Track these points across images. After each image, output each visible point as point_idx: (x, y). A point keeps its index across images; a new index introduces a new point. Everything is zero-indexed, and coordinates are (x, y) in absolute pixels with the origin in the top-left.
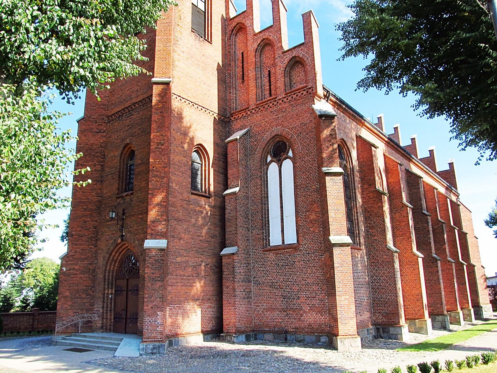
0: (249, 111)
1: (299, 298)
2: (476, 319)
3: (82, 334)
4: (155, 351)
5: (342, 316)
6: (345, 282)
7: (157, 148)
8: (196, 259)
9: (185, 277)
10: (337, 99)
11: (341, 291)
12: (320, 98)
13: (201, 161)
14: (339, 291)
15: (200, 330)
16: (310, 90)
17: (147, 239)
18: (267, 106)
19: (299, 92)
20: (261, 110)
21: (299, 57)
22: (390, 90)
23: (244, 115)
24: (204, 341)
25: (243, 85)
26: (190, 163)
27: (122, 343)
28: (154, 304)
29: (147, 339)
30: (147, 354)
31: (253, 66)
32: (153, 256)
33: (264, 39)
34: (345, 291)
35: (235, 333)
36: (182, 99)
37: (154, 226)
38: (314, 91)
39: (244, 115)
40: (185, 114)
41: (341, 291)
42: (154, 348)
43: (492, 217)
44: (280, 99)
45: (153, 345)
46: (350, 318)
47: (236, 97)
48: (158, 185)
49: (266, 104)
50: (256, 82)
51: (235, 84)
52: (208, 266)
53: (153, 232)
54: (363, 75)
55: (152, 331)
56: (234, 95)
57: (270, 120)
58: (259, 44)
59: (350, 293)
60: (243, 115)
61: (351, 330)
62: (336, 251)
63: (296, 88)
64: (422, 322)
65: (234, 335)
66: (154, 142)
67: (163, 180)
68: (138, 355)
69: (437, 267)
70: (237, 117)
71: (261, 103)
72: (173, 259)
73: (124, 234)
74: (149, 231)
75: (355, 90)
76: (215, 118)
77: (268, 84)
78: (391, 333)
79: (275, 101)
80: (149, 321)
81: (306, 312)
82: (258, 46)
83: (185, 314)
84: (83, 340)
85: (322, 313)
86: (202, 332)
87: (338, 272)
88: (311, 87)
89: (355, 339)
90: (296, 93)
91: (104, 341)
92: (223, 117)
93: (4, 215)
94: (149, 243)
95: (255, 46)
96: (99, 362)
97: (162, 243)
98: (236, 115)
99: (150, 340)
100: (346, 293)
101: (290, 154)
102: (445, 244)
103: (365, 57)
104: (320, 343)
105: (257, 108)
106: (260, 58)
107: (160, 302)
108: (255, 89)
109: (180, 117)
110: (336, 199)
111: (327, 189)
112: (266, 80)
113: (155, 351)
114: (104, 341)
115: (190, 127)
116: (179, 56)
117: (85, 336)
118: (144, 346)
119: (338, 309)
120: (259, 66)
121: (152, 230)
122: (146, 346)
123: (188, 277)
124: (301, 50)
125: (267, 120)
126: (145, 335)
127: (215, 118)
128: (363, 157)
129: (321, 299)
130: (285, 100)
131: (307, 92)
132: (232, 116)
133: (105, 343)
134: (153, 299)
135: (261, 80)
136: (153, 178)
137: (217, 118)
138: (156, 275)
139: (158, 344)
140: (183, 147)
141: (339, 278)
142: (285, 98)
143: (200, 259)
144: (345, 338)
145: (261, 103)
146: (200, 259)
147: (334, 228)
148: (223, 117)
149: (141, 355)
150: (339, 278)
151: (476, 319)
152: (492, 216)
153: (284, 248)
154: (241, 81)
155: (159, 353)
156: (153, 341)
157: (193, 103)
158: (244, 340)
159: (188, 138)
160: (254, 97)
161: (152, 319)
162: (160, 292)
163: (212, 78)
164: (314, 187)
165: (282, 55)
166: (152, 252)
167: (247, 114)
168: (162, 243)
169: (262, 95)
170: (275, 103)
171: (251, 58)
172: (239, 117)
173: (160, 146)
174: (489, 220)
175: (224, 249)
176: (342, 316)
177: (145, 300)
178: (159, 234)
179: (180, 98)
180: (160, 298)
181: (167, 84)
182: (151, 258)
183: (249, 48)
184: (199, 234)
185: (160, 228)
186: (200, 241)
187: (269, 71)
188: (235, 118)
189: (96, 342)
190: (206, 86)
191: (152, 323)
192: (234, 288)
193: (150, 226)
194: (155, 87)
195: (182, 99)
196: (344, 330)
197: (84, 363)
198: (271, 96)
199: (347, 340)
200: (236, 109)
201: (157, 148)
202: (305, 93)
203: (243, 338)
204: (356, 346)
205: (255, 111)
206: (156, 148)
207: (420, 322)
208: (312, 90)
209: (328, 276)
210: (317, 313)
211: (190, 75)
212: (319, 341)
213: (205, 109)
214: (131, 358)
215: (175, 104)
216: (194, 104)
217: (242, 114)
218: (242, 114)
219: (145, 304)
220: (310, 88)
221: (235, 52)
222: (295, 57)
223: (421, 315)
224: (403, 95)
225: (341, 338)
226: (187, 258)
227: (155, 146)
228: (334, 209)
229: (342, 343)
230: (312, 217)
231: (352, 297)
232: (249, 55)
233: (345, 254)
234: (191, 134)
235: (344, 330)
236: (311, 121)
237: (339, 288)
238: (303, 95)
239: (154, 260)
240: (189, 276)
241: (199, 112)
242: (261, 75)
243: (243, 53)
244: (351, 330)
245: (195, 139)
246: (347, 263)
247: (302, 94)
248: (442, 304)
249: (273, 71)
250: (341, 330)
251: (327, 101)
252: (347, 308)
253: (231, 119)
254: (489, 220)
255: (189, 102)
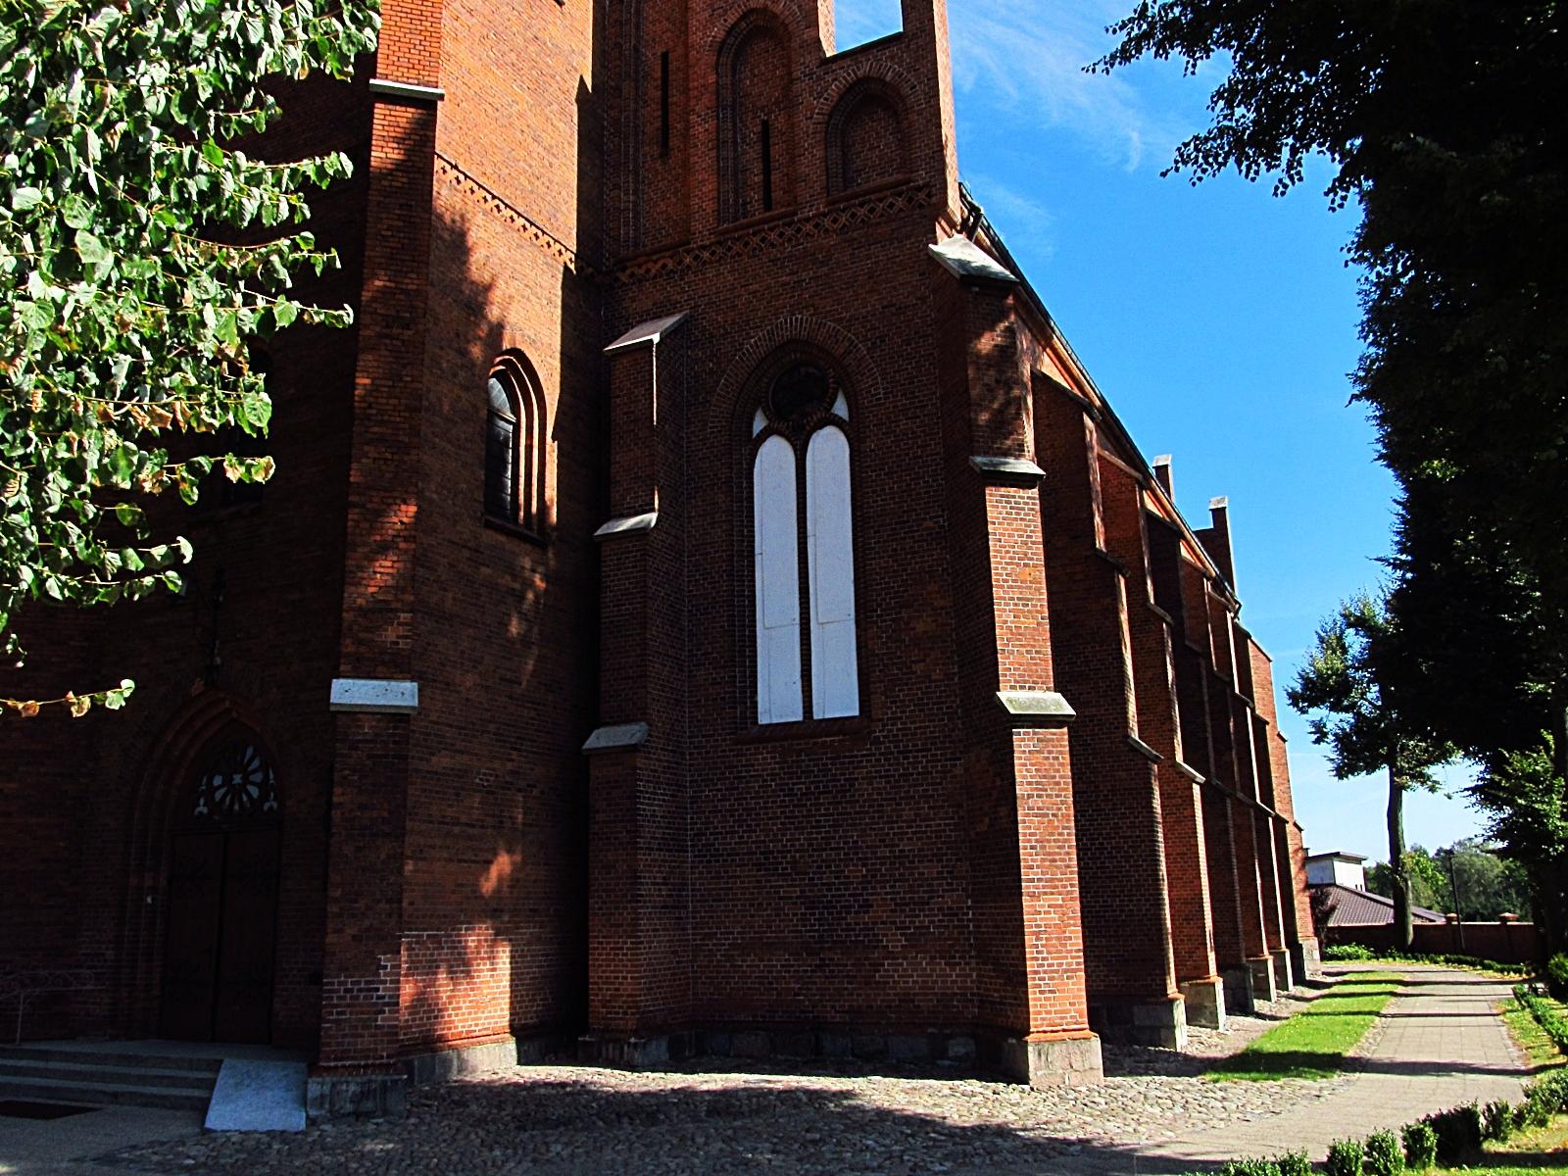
0: (688, 252)
1: (867, 906)
2: (1295, 983)
3: (27, 1046)
4: (369, 1105)
5: (1042, 965)
6: (1052, 847)
7: (387, 336)
8: (496, 765)
9: (457, 830)
10: (992, 241)
11: (1039, 880)
12: (952, 225)
13: (516, 412)
14: (1033, 880)
15: (505, 1022)
16: (922, 195)
17: (338, 677)
18: (757, 240)
19: (881, 200)
20: (733, 252)
21: (881, 80)
22: (1291, 178)
23: (670, 266)
24: (519, 1063)
25: (664, 163)
26: (484, 414)
27: (224, 1080)
28: (367, 923)
29: (335, 1060)
30: (335, 1117)
31: (707, 99)
32: (367, 741)
33: (752, 11)
34: (1052, 880)
35: (636, 1033)
36: (462, 177)
37: (368, 630)
38: (934, 200)
39: (670, 266)
40: (473, 237)
41: (1039, 880)
42: (362, 1096)
43: (1307, 682)
44: (808, 220)
45: (363, 1084)
46: (1066, 971)
47: (636, 204)
48: (388, 475)
49: (754, 234)
50: (718, 157)
51: (636, 159)
52: (535, 792)
53: (362, 649)
54: (1207, 121)
55: (356, 1027)
56: (632, 198)
57: (769, 287)
58: (733, 26)
59: (1065, 887)
60: (664, 266)
61: (1069, 1011)
62: (1024, 742)
63: (865, 187)
64: (1202, 988)
65: (633, 1040)
66: (376, 313)
67: (406, 458)
68: (303, 1125)
69: (1225, 816)
70: (642, 271)
71: (736, 229)
72: (421, 759)
73: (218, 660)
74: (348, 646)
75: (1164, 174)
76: (566, 268)
77: (757, 167)
78: (1137, 1023)
79: (789, 225)
80: (347, 991)
81: (892, 956)
82: (729, 33)
83: (461, 967)
84: (37, 1069)
85: (954, 957)
86: (514, 1030)
87: (1027, 815)
88: (926, 185)
89: (1085, 1045)
90: (870, 200)
91: (135, 1071)
92: (590, 270)
93: (104, 321)
94: (347, 691)
95: (717, 31)
96: (155, 1158)
97: (402, 693)
98: (640, 266)
99: (348, 1063)
100: (1052, 884)
101: (841, 408)
102: (1231, 749)
103: (1190, 69)
104: (947, 1063)
105: (720, 243)
106: (733, 76)
107: (390, 915)
108: (713, 179)
109: (458, 244)
110: (1018, 565)
111: (990, 528)
112: (753, 153)
113: (369, 1105)
114: (135, 1071)
115: (488, 288)
116: (456, 23)
117: (45, 1055)
118: (327, 1089)
119: (1029, 940)
120: (730, 105)
121: (360, 642)
122: (334, 1085)
123: (470, 831)
124: (892, 58)
125: (756, 287)
126: (329, 1045)
127: (566, 268)
128: (1052, 446)
129: (949, 908)
130: (827, 222)
131: (910, 200)
132: (624, 270)
133: (142, 1080)
134: (361, 904)
135: (735, 150)
136: (366, 448)
137: (572, 267)
138: (375, 814)
139: (380, 1078)
140: (464, 353)
141: (1031, 835)
142: (824, 215)
143: (509, 766)
144: (1052, 1042)
145: (736, 229)
146: (509, 766)
147: (1011, 663)
148: (590, 270)
149: (312, 1122)
150: (1031, 835)
151: (1295, 983)
152: (1309, 678)
153: (809, 730)
154: (656, 151)
155: (386, 1112)
156: (359, 1067)
157: (497, 202)
158: (665, 1057)
159: (485, 327)
160: (710, 206)
161: (359, 983)
162: (392, 879)
163: (561, 125)
164: (930, 524)
165: (820, 72)
166: (363, 727)
167: (680, 262)
168: (402, 693)
169: (736, 201)
170: (789, 232)
171: (704, 74)
172: (648, 271)
173: (396, 331)
174: (1299, 689)
175: (596, 732)
176: (1042, 965)
177: (333, 909)
178: (387, 658)
179: (455, 173)
180: (389, 901)
181: (427, 104)
182: (357, 749)
183: (695, 38)
184: (509, 675)
185: (390, 634)
186: (510, 697)
187: (765, 124)
188: (632, 275)
189: (103, 1077)
190: (540, 150)
191: (357, 997)
192: (636, 871)
193: (350, 629)
194: (380, 109)
195: (462, 177)
196: (1047, 1012)
197: (88, 1165)
198: (768, 207)
199: (1057, 1048)
200: (636, 245)
201: (387, 336)
202: (900, 202)
203: (659, 1049)
204: (1087, 1067)
205: (713, 253)
206: (380, 336)
207: (1194, 989)
208: (929, 196)
209: (983, 827)
210: (933, 958)
211: (490, 100)
212: (943, 1055)
213: (534, 230)
214: (282, 1136)
215: (446, 194)
216: (502, 206)
217: (660, 264)
218: (660, 264)
219: (330, 926)
220: (919, 189)
221: (636, 49)
222: (867, 79)
223: (1196, 968)
224: (1333, 201)
225: (1038, 1043)
226: (465, 757)
227: (378, 329)
228: (1012, 599)
229: (1043, 1058)
230: (920, 627)
231: (1072, 899)
232: (692, 61)
233: (1050, 752)
234: (494, 313)
235: (1047, 1012)
236: (923, 299)
237: (1032, 867)
238: (895, 209)
239: (369, 757)
240: (473, 826)
241: (516, 235)
242: (735, 133)
243: (665, 56)
244: (1069, 1011)
245: (507, 334)
246: (1058, 784)
247: (891, 205)
248: (1236, 934)
249: (779, 122)
250: (1039, 1013)
251: (970, 237)
252: (1058, 939)
253: (617, 279)
254: (1299, 689)
255: (485, 194)
